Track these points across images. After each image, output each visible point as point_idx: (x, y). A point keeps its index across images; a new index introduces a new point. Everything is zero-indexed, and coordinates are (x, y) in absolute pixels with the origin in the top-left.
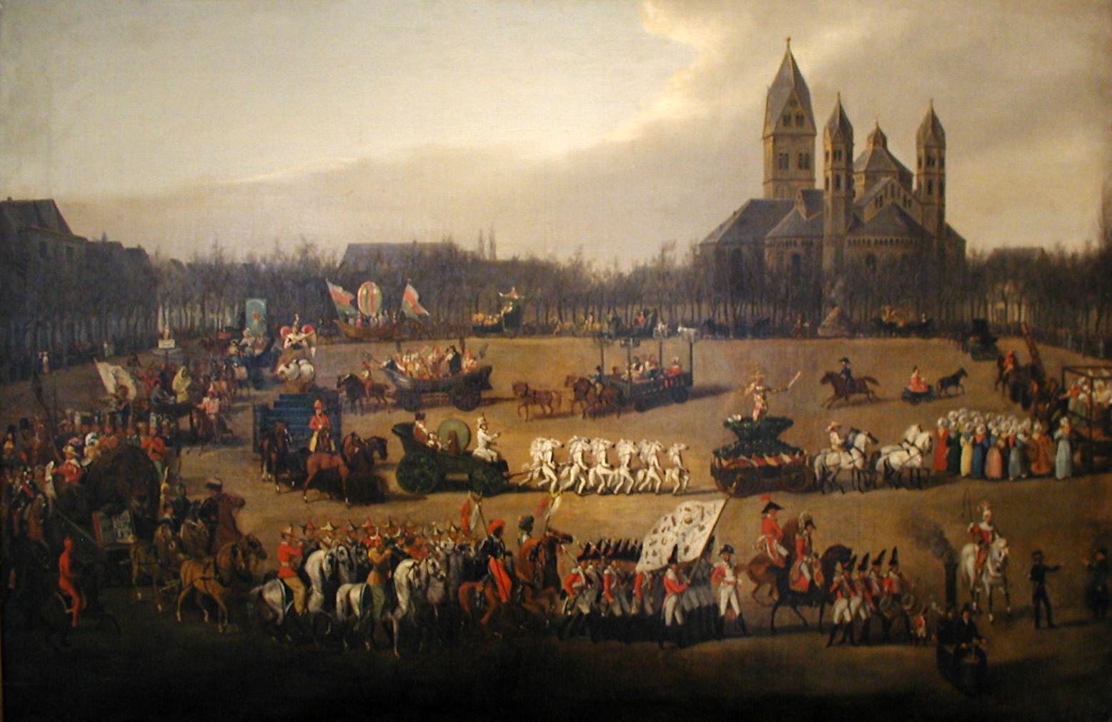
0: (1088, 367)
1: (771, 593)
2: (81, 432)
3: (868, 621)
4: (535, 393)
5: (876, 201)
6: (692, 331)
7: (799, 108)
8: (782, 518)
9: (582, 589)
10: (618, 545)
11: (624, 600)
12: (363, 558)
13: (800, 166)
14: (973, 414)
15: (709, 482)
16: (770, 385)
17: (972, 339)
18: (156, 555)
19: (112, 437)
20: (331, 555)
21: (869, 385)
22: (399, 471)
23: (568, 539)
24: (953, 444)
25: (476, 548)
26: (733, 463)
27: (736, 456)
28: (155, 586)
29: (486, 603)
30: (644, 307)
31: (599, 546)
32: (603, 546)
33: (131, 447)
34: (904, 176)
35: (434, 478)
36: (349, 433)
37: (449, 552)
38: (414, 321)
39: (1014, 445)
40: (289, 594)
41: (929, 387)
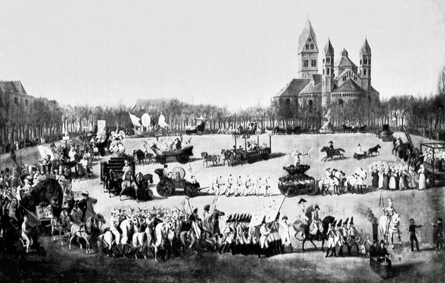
0: (431, 144)
1: (302, 235)
2: (32, 173)
3: (342, 247)
4: (210, 156)
5: (343, 78)
6: (271, 132)
7: (312, 42)
8: (307, 205)
9: (228, 234)
10: (242, 216)
11: (244, 238)
12: (144, 222)
13: (312, 66)
14: (383, 163)
15: (278, 192)
16: (300, 152)
17: (382, 133)
18: (61, 223)
19: (44, 176)
20: (131, 221)
21: (341, 152)
22: (158, 187)
23: (223, 214)
24: (375, 175)
25: (187, 217)
26: (287, 183)
27: (288, 180)
28: (60, 235)
29: (191, 239)
30: (251, 122)
31: (235, 217)
32: (236, 216)
33: (52, 179)
34: (354, 68)
35: (171, 191)
36: (139, 172)
37: (176, 219)
38: (164, 129)
39: (401, 175)
40: (114, 237)
41: (365, 152)
